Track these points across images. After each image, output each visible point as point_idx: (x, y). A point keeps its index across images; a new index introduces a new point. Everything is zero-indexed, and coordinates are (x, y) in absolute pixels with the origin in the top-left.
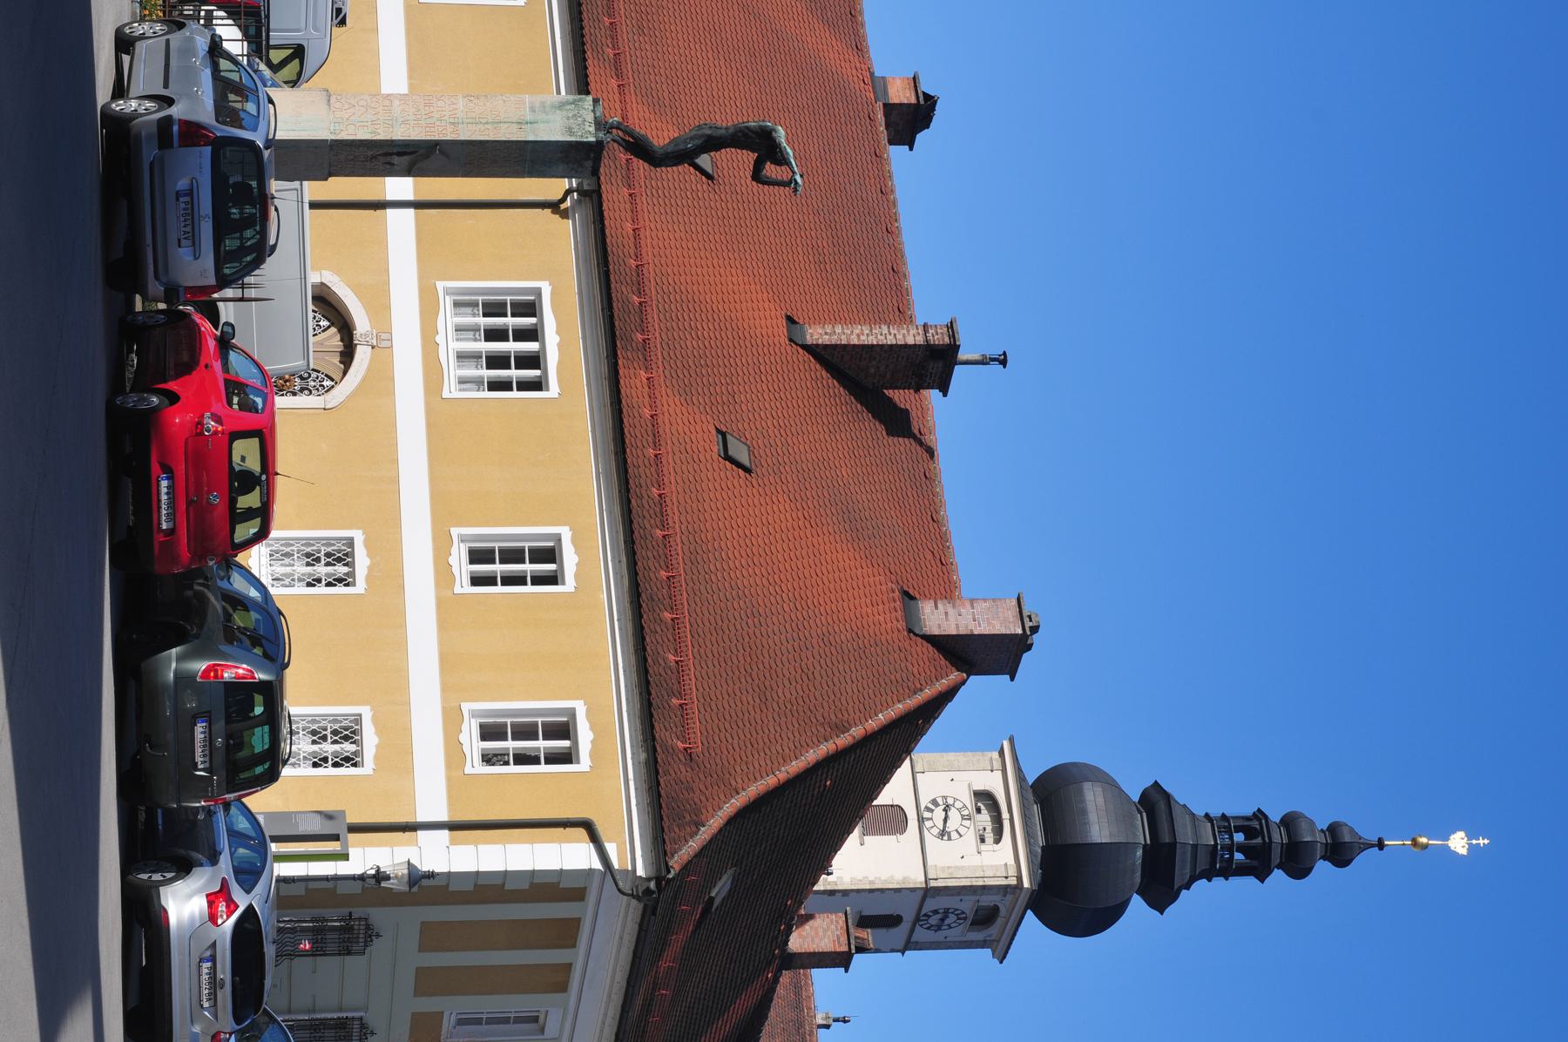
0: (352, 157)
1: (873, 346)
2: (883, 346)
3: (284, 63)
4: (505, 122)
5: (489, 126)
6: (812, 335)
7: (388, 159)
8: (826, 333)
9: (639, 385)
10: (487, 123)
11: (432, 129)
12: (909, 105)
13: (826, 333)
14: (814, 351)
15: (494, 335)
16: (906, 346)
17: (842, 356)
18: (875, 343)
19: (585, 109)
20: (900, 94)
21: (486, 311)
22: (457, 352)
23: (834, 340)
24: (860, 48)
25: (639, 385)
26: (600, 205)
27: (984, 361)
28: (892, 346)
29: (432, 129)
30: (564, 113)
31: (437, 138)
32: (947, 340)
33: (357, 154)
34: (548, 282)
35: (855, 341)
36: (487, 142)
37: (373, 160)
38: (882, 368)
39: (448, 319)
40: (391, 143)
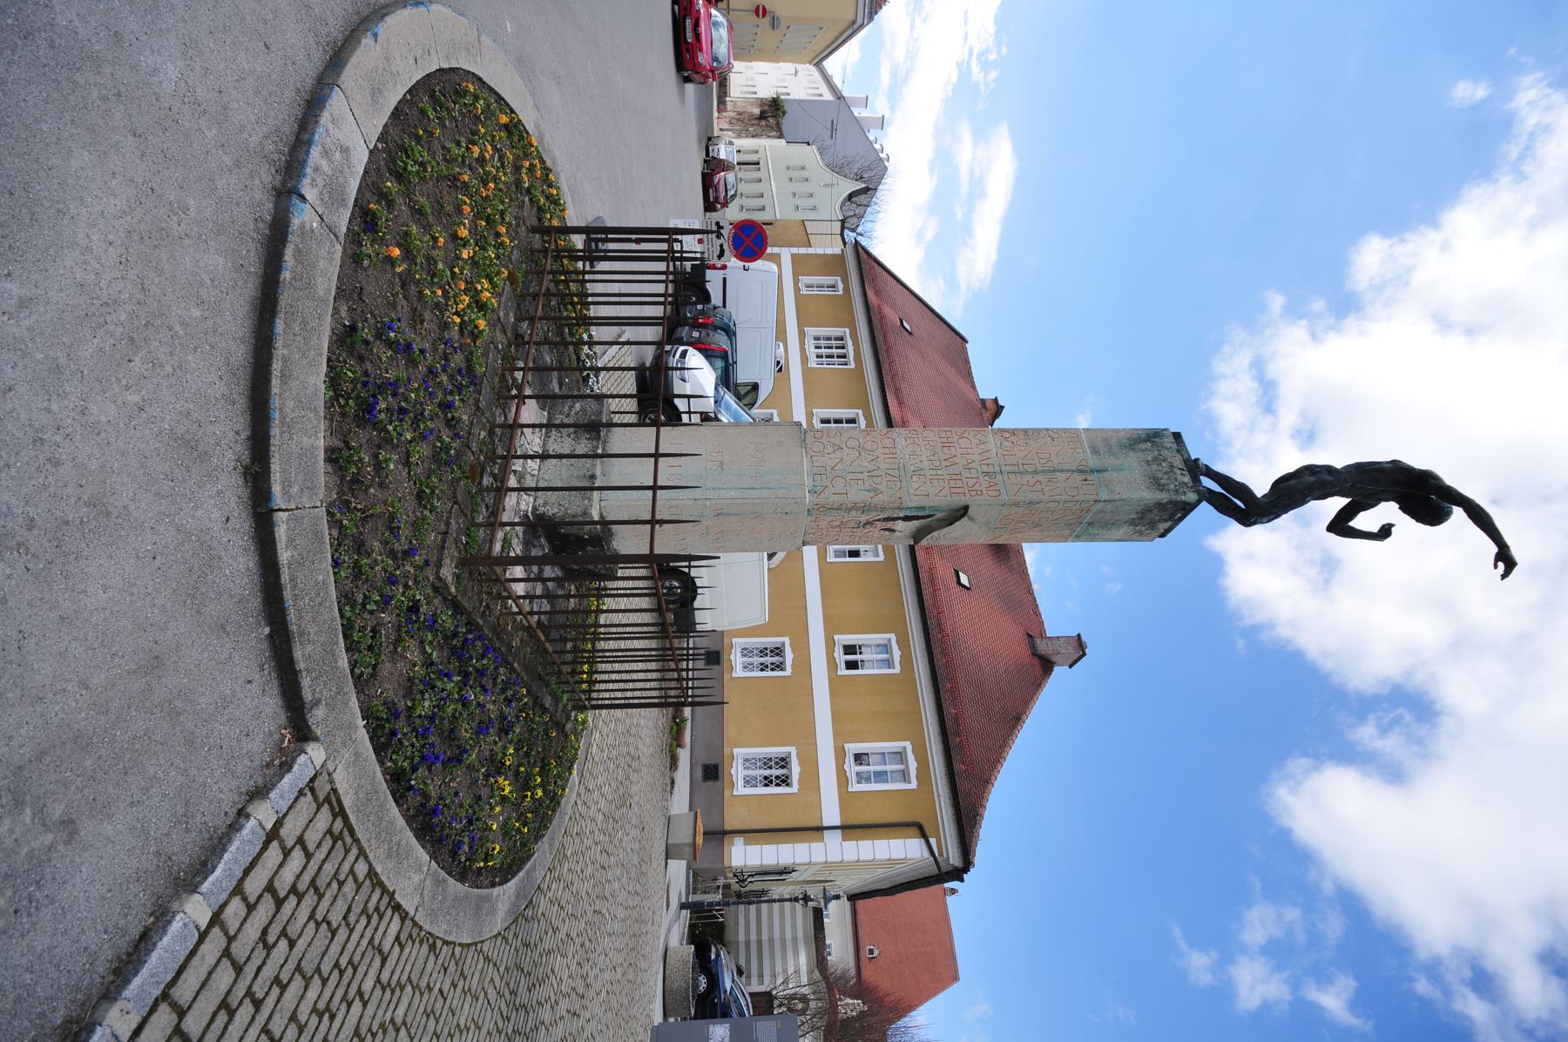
0: (838, 523)
3: (747, 394)
4: (1062, 471)
5: (1040, 477)
7: (889, 525)
10: (1035, 472)
11: (959, 484)
19: (1166, 448)
24: (974, 387)
29: (959, 484)
30: (1141, 455)
37: (868, 526)
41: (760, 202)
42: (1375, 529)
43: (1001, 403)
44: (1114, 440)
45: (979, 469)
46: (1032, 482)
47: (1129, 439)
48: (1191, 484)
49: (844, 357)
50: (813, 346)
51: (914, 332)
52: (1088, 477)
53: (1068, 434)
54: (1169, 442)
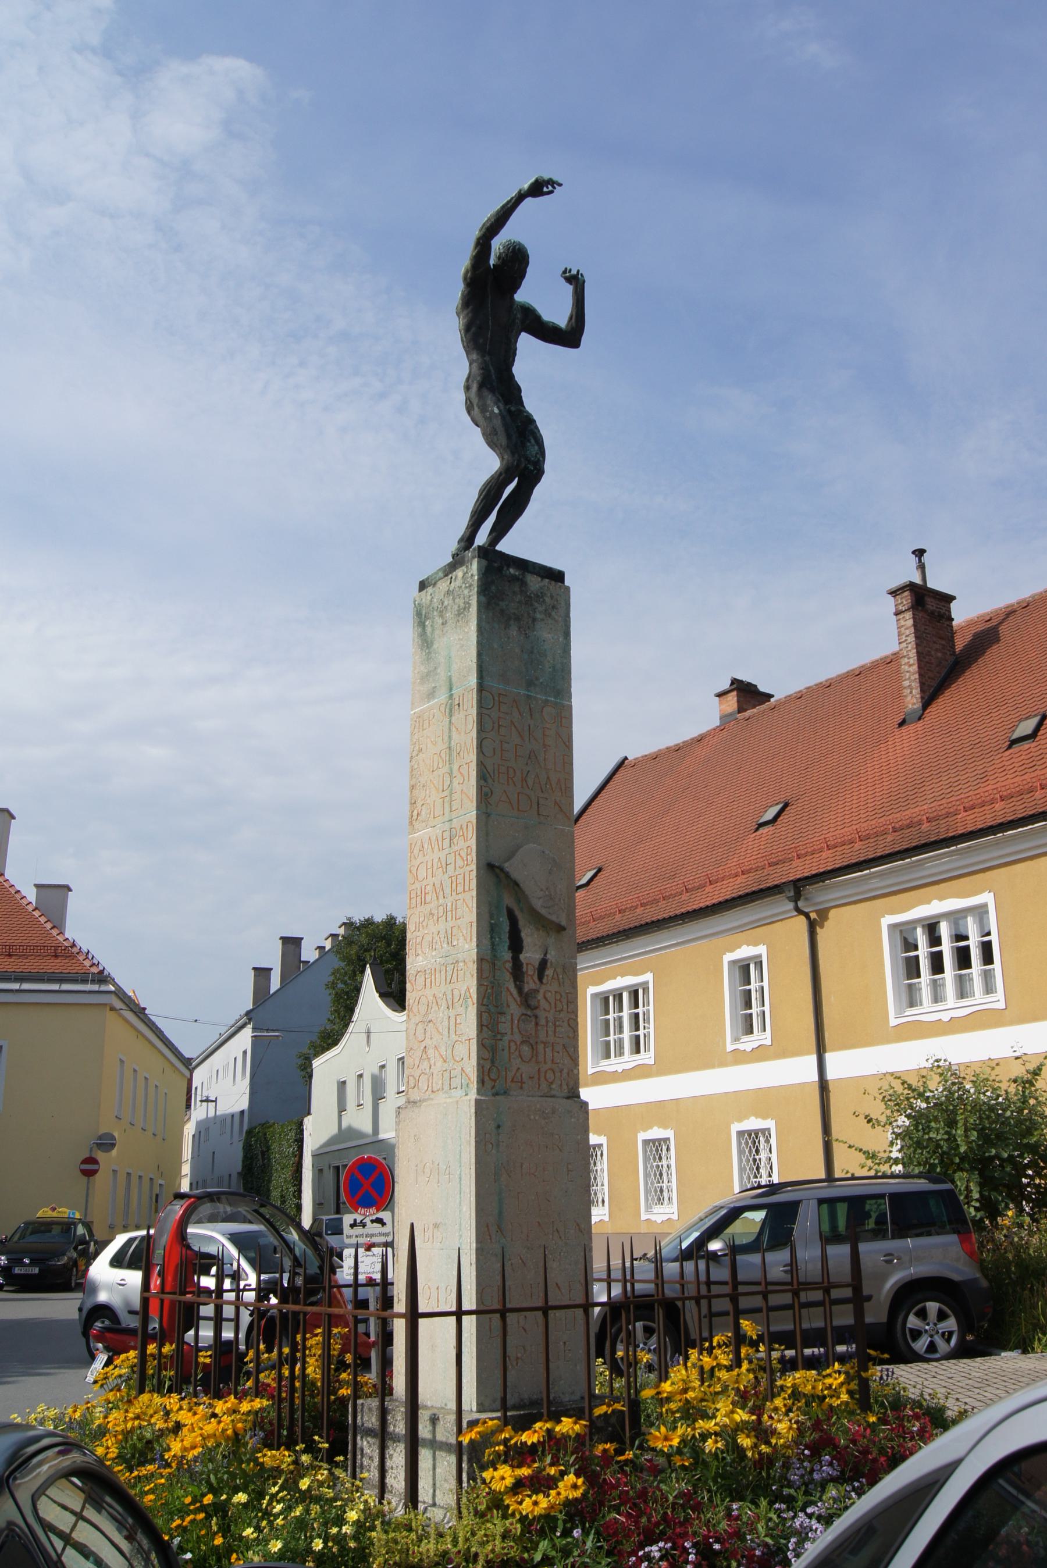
0: (525, 1048)
1: (918, 652)
2: (917, 645)
4: (450, 737)
5: (455, 767)
6: (914, 704)
7: (530, 972)
8: (911, 692)
9: (973, 816)
11: (460, 878)
12: (738, 696)
13: (911, 692)
14: (927, 703)
15: (937, 965)
16: (915, 625)
17: (929, 678)
18: (915, 651)
20: (732, 702)
21: (915, 974)
22: (957, 999)
23: (916, 685)
25: (973, 816)
26: (807, 878)
27: (922, 567)
28: (916, 637)
29: (460, 878)
30: (437, 632)
31: (474, 867)
32: (906, 593)
33: (518, 1038)
34: (882, 919)
35: (915, 668)
36: (481, 766)
37: (533, 1003)
38: (938, 646)
39: (927, 1011)
40: (486, 964)
41: (134, 1180)
42: (569, 289)
43: (726, 685)
44: (422, 668)
45: (447, 851)
46: (460, 779)
47: (422, 649)
48: (464, 568)
49: (635, 994)
50: (619, 1060)
51: (783, 797)
52: (457, 703)
53: (416, 730)
54: (426, 596)
